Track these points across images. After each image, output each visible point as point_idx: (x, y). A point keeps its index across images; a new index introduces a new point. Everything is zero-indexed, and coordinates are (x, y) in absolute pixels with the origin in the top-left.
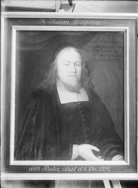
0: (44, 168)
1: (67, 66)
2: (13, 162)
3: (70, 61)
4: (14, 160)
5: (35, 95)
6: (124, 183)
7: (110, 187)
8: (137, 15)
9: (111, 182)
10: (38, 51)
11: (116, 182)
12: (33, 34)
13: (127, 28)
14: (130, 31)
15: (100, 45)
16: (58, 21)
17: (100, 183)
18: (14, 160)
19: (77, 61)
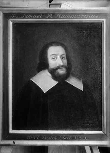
0: (38, 137)
1: (54, 60)
2: (11, 131)
3: (55, 53)
4: (12, 130)
5: (26, 93)
6: (101, 148)
7: (90, 152)
8: (108, 9)
9: (91, 148)
10: (29, 55)
11: (96, 146)
12: (7, 87)
13: (104, 20)
14: (105, 22)
15: (84, 37)
16: (34, 16)
17: (82, 149)
18: (12, 130)
19: (64, 54)
